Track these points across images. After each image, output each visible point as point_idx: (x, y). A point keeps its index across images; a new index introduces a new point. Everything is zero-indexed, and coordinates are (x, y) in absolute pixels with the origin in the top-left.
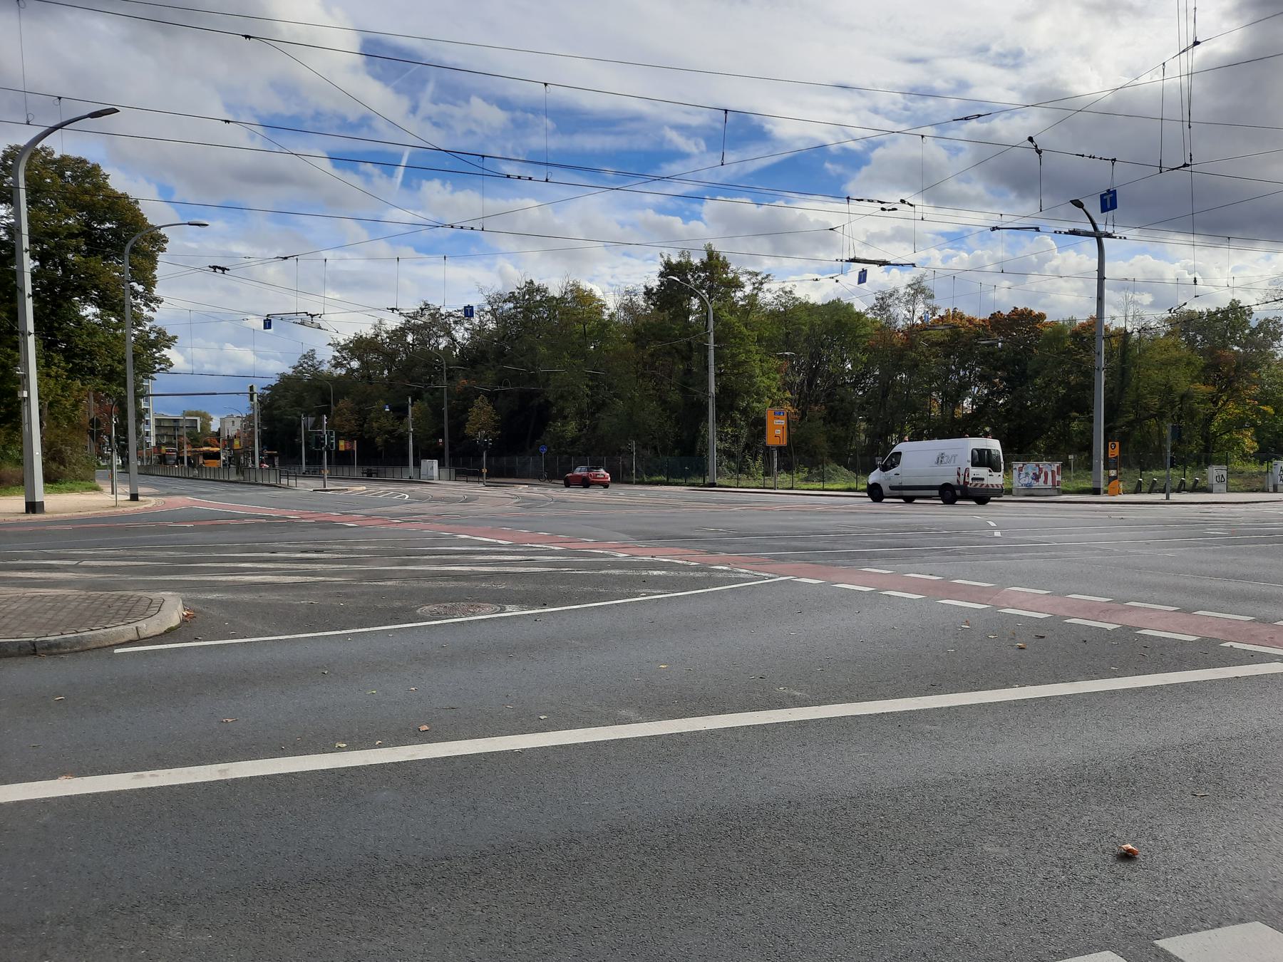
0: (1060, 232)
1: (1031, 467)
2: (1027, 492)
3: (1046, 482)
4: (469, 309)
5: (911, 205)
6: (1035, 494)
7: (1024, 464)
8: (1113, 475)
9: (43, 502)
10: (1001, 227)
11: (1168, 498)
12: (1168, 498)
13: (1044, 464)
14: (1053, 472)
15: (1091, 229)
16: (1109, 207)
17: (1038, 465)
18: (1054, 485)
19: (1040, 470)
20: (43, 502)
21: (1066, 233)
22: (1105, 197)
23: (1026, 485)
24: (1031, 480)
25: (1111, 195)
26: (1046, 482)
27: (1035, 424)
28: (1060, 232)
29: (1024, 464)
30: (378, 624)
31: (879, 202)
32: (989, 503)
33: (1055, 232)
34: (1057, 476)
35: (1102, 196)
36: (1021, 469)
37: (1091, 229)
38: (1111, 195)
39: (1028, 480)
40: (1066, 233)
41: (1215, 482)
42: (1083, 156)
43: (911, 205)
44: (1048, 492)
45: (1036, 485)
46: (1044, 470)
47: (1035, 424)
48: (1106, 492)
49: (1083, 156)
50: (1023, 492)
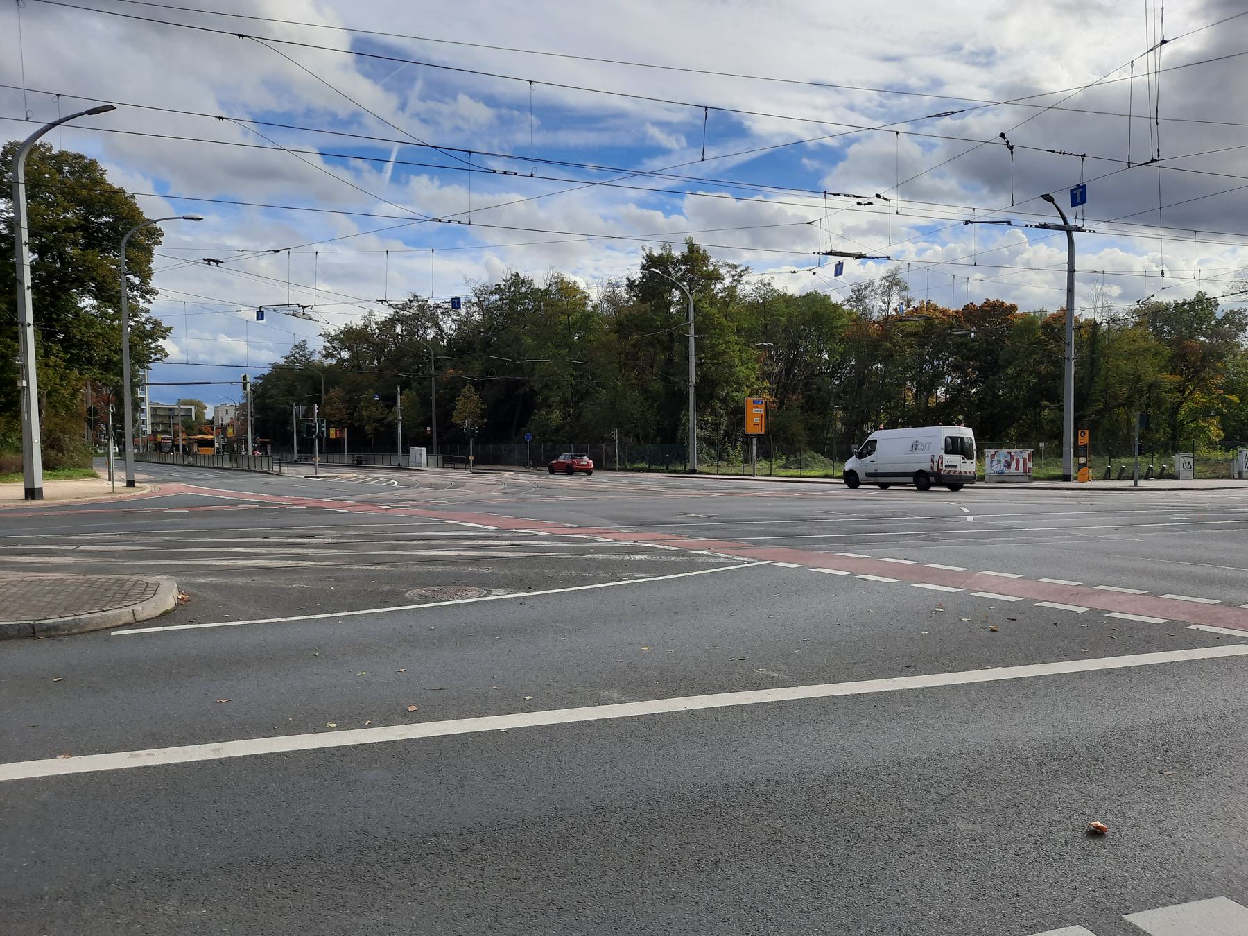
0: (1031, 226)
1: (1003, 454)
2: (999, 479)
3: (1017, 469)
4: (456, 301)
5: (886, 200)
6: (1007, 480)
7: (996, 452)
8: (1082, 462)
9: (42, 488)
10: (973, 221)
11: (1136, 485)
12: (1136, 485)
13: (1016, 452)
14: (1024, 459)
15: (1061, 223)
16: (1078, 201)
17: (1010, 453)
18: (1025, 472)
19: (1012, 457)
20: (42, 488)
21: (1036, 227)
22: (1075, 192)
23: (998, 472)
24: (1002, 467)
25: (1081, 190)
26: (1017, 469)
27: (1007, 412)
28: (1031, 226)
29: (996, 452)
30: (368, 607)
31: (855, 196)
32: (962, 490)
33: (1027, 226)
34: (1028, 464)
35: (1072, 191)
36: (993, 457)
37: (1061, 223)
38: (1081, 190)
39: (1000, 467)
40: (1036, 227)
41: (1182, 469)
42: (1053, 152)
43: (886, 200)
44: (1020, 479)
45: (1007, 472)
46: (1015, 457)
47: (1007, 412)
48: (1076, 479)
49: (1053, 152)
50: (995, 479)
